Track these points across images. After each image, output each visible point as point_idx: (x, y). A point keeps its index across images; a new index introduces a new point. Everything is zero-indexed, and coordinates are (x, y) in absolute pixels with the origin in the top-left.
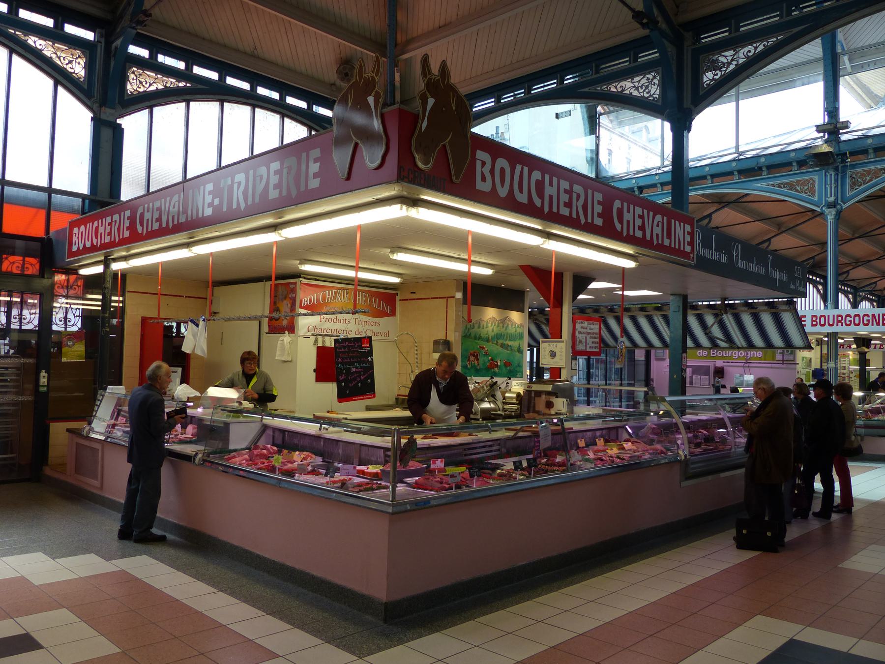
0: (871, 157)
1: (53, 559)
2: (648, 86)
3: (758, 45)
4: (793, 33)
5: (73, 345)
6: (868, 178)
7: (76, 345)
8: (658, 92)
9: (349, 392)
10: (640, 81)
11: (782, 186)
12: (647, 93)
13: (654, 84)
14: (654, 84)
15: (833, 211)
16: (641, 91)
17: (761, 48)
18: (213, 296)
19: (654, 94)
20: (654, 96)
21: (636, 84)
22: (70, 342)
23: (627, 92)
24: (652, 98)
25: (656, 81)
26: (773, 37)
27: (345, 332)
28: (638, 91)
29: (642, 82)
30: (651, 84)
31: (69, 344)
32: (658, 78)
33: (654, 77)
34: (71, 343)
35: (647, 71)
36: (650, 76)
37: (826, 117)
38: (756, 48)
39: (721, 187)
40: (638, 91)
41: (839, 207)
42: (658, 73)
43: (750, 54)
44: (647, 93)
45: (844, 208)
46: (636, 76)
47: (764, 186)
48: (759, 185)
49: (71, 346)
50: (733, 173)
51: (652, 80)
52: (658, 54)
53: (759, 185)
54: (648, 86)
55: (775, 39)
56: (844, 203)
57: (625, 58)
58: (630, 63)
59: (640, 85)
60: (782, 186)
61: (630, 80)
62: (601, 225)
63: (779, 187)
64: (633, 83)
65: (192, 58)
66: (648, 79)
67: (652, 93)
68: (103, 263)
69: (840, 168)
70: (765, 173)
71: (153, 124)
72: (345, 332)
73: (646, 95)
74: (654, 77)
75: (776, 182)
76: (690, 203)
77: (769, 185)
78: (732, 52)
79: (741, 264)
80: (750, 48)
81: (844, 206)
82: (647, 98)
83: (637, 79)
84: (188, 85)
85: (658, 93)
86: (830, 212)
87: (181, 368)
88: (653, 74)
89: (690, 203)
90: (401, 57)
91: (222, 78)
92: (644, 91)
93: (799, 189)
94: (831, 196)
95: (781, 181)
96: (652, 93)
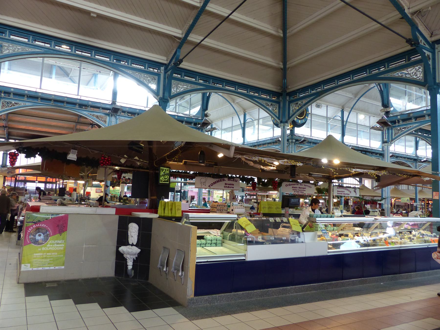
1: (130, 311)
2: (416, 73)
5: (46, 239)
7: (51, 240)
8: (421, 75)
10: (411, 70)
13: (420, 72)
14: (420, 72)
18: (19, 253)
19: (419, 77)
20: (420, 77)
21: (409, 72)
22: (40, 235)
24: (418, 79)
25: (420, 70)
29: (412, 71)
30: (418, 71)
31: (37, 237)
32: (422, 68)
34: (42, 237)
35: (415, 65)
36: (417, 68)
37: (63, 215)
42: (421, 66)
47: (87, 114)
49: (40, 242)
51: (418, 70)
52: (420, 57)
54: (416, 73)
58: (406, 62)
61: (406, 70)
64: (407, 71)
67: (418, 76)
71: (194, 50)
74: (420, 68)
77: (91, 115)
79: (332, 169)
82: (416, 79)
83: (409, 70)
84: (246, 176)
85: (422, 76)
88: (419, 66)
96: (418, 76)
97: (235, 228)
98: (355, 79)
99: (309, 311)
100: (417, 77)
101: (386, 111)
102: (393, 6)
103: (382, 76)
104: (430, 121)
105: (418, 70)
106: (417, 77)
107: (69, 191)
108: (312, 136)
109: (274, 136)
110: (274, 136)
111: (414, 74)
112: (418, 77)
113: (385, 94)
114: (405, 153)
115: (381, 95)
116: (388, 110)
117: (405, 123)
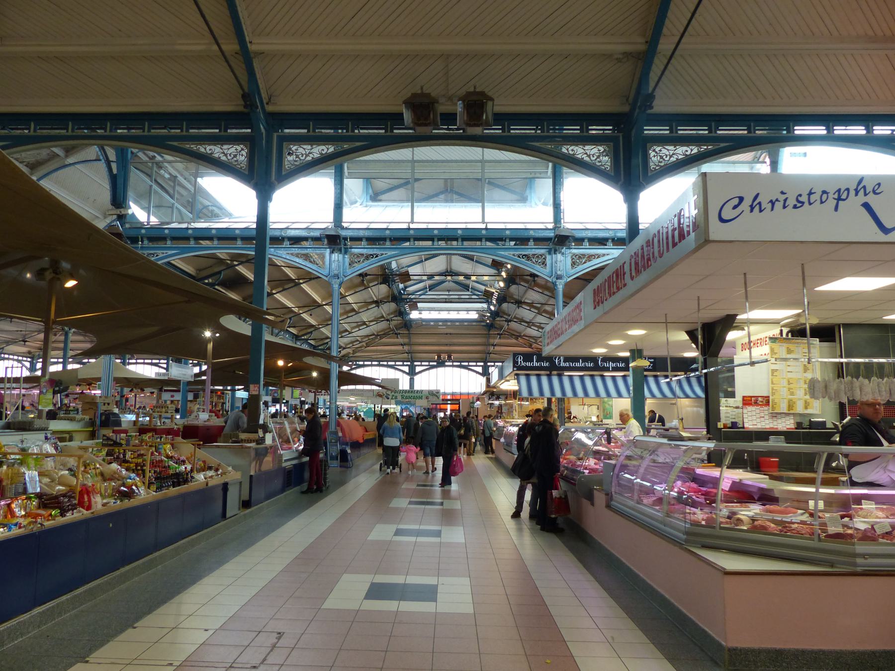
0: (364, 243)
3: (330, 146)
4: (355, 146)
6: (584, 261)
9: (113, 525)
11: (521, 256)
12: (599, 162)
14: (242, 155)
16: (229, 158)
17: (695, 151)
20: (606, 166)
21: (588, 152)
23: (579, 156)
26: (704, 145)
28: (227, 157)
33: (654, 151)
36: (239, 148)
38: (692, 150)
39: (473, 250)
40: (227, 157)
43: (324, 152)
44: (599, 162)
48: (503, 253)
51: (240, 151)
53: (503, 253)
54: (660, 156)
55: (705, 147)
56: (345, 277)
57: (247, 128)
60: (521, 256)
61: (220, 146)
63: (519, 257)
65: (429, 362)
68: (270, 233)
69: (343, 249)
70: (169, 242)
73: (598, 164)
74: (242, 149)
75: (512, 253)
78: (309, 147)
80: (323, 147)
81: (346, 279)
82: (235, 165)
87: (813, 501)
93: (534, 260)
95: (520, 253)
97: (840, 371)
98: (513, 134)
99: (174, 628)
100: (600, 164)
101: (119, 213)
102: (229, 15)
103: (175, 144)
104: (254, 249)
105: (240, 151)
106: (600, 164)
107: (146, 224)
108: (486, 220)
111: (232, 155)
112: (601, 165)
113: (120, 181)
114: (483, 222)
115: (111, 181)
116: (123, 213)
117: (151, 245)
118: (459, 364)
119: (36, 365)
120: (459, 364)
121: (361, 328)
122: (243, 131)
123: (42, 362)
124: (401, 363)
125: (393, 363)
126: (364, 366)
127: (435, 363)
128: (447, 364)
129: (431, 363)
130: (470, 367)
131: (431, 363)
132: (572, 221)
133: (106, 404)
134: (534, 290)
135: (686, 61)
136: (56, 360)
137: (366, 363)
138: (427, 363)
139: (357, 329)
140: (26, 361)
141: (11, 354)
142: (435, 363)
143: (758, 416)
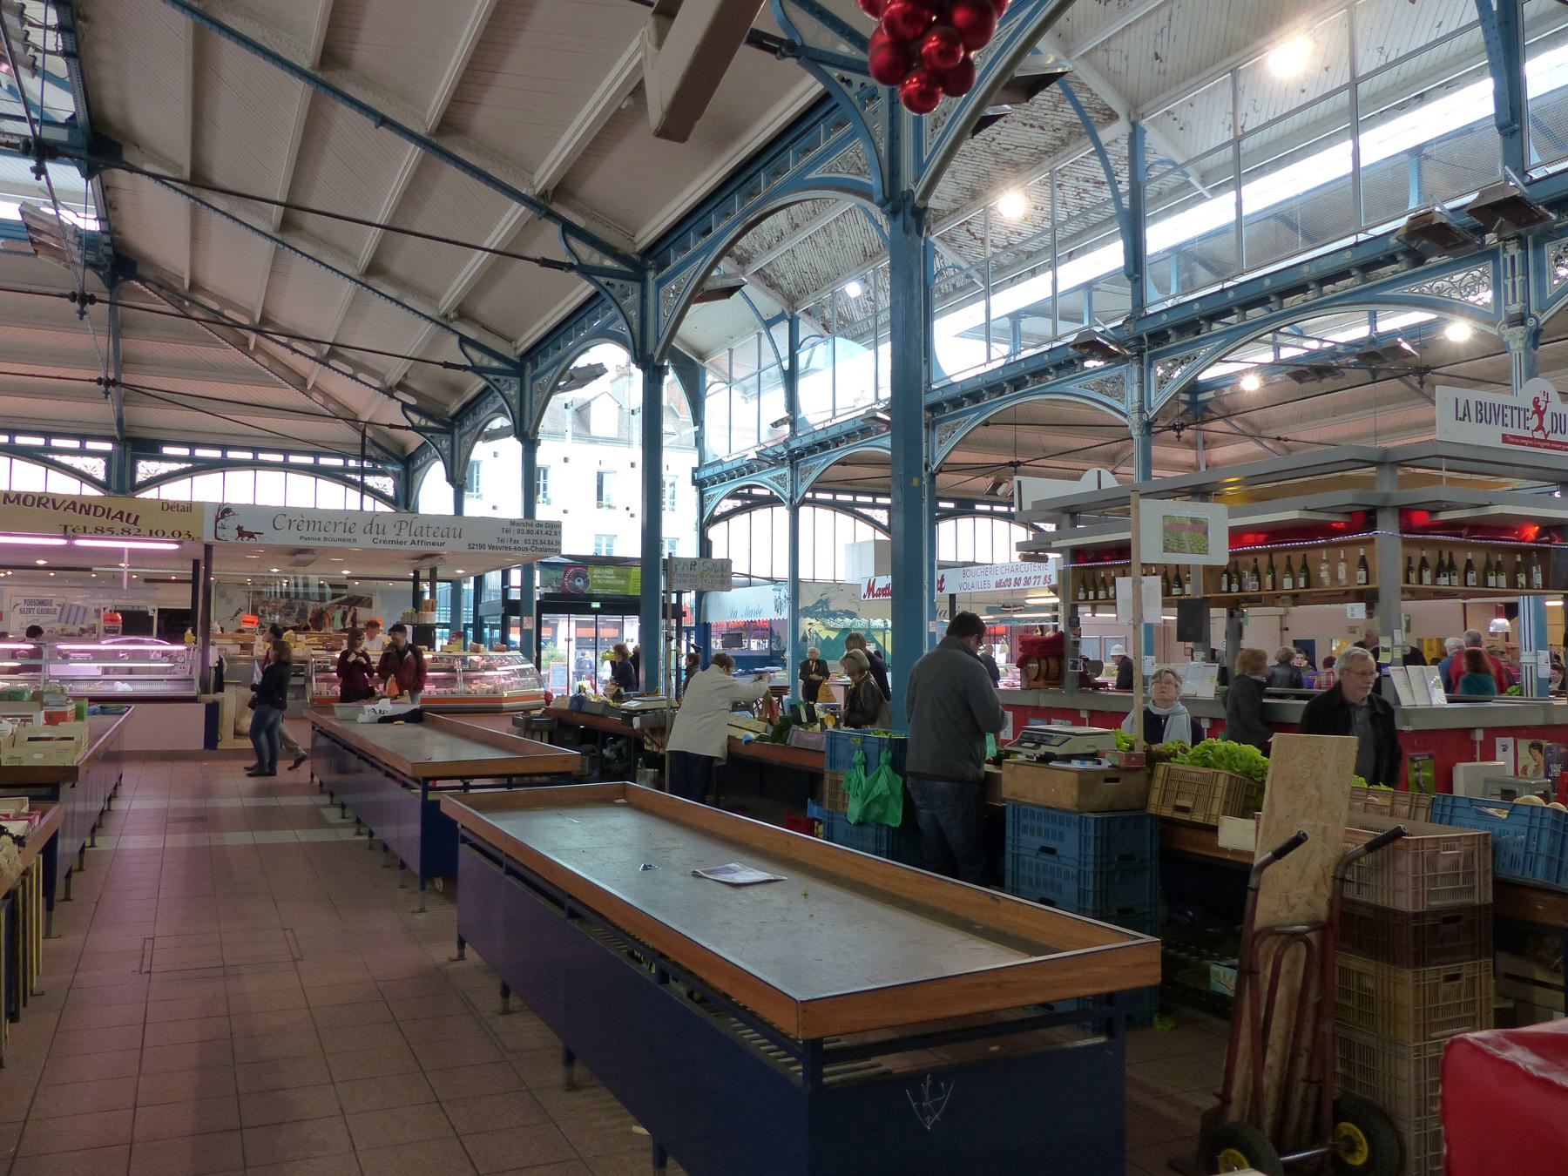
10: (1461, 280)
15: (1519, 331)
27: (340, 527)
36: (1476, 273)
41: (1531, 323)
45: (1542, 322)
46: (1456, 274)
50: (1395, 258)
56: (1543, 312)
59: (1463, 285)
62: (639, 555)
65: (192, 445)
66: (1474, 277)
72: (340, 527)
76: (1100, 486)
81: (1543, 319)
86: (1513, 335)
89: (1100, 486)
90: (489, 426)
91: (224, 455)
92: (1469, 293)
94: (1514, 302)
109: (709, 459)
110: (709, 459)
118: (309, 460)
119: (134, 471)
120: (309, 460)
121: (361, 376)
122: (1297, 1156)
123: (1328, 570)
124: (75, 444)
125: (849, 498)
126: (223, 465)
127: (951, 505)
128: (978, 507)
129: (200, 453)
130: (57, 458)
131: (200, 453)
132: (290, 313)
133: (630, 512)
134: (357, 380)
135: (272, 272)
136: (217, 454)
137: (231, 455)
138: (185, 452)
139: (349, 370)
140: (874, 506)
141: (1001, 504)
142: (951, 505)
143: (278, 590)
